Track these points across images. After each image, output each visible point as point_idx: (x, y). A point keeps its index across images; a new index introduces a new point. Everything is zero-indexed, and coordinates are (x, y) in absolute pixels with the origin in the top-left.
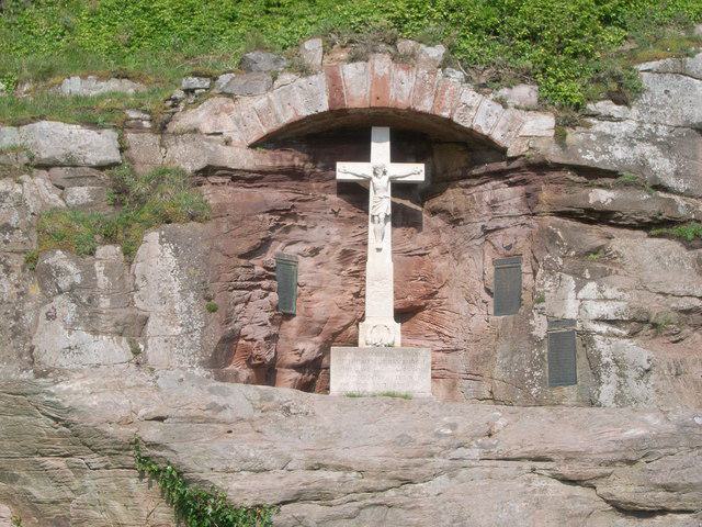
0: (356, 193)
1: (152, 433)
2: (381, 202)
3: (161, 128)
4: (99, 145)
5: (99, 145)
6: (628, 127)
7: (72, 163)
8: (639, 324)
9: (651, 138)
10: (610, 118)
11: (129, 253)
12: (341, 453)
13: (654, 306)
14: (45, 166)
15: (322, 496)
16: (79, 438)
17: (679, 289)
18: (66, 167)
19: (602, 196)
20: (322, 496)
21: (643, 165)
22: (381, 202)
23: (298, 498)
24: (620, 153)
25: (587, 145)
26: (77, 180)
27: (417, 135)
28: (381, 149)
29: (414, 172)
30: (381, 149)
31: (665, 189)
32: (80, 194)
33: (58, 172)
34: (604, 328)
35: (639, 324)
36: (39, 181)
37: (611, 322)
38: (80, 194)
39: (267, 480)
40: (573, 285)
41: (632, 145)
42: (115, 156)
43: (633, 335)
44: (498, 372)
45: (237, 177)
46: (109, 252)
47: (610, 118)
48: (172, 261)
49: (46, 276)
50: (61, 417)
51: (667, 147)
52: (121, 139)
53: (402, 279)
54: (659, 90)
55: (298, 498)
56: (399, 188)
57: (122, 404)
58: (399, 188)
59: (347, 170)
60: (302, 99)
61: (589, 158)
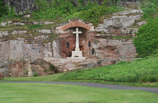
0: (75, 34)
1: (50, 62)
2: (77, 36)
3: (55, 29)
4: (49, 31)
5: (49, 31)
6: (102, 27)
7: (46, 34)
8: (100, 49)
9: (105, 28)
10: (100, 26)
11: (52, 43)
12: (62, 63)
13: (102, 46)
14: (44, 34)
15: (60, 65)
16: (45, 62)
17: (105, 44)
18: (45, 34)
19: (98, 35)
20: (60, 65)
21: (103, 31)
22: (77, 36)
23: (59, 66)
24: (101, 30)
25: (98, 29)
26: (46, 35)
27: (80, 29)
28: (77, 29)
29: (81, 32)
30: (77, 29)
31: (106, 33)
32: (47, 37)
33: (45, 35)
34: (96, 49)
35: (100, 49)
36: (43, 36)
37: (97, 48)
38: (47, 37)
39: (57, 65)
40: (94, 45)
41: (102, 29)
42: (50, 33)
43: (99, 49)
44: (88, 53)
45: (62, 34)
46: (50, 43)
47: (100, 26)
48: (56, 44)
49: (44, 46)
50: (44, 61)
51: (107, 29)
52: (51, 31)
53: (80, 44)
54: (106, 22)
55: (59, 66)
56: (79, 34)
57: (48, 60)
58: (79, 34)
59: (74, 33)
60: (68, 25)
61: (98, 31)
